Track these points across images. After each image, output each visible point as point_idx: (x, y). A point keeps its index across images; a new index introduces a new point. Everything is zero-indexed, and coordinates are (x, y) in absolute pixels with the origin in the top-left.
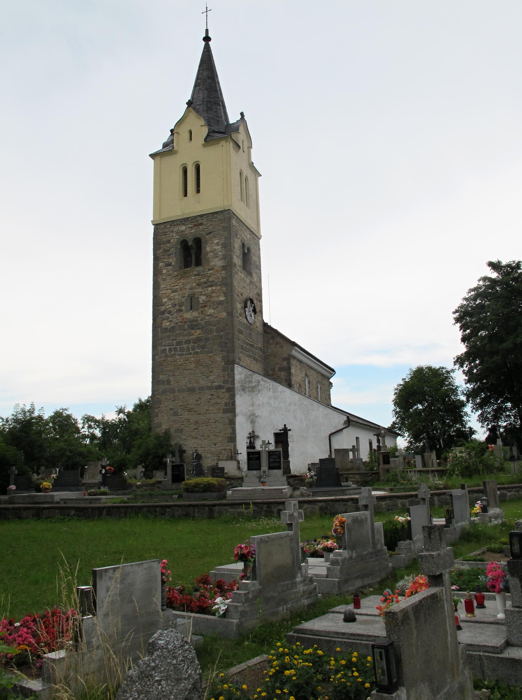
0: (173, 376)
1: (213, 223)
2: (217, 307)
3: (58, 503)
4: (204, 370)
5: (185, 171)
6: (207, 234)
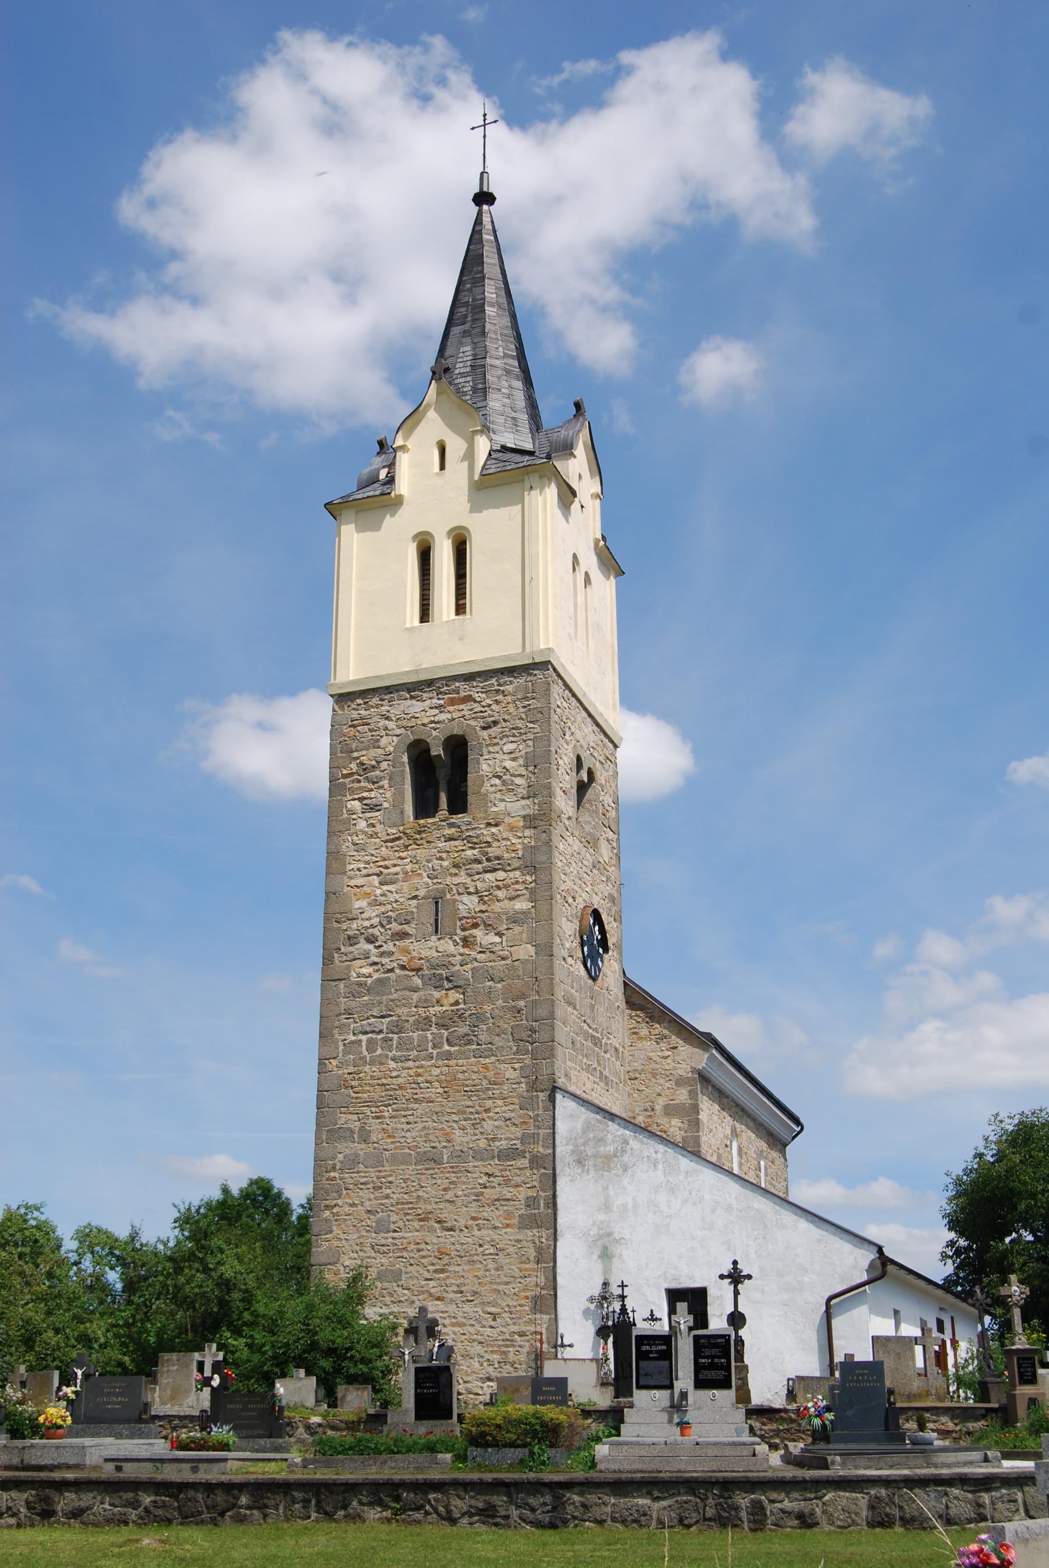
0: (378, 1118)
1: (500, 697)
2: (508, 929)
3: (96, 1468)
4: (469, 1103)
5: (425, 556)
6: (484, 728)
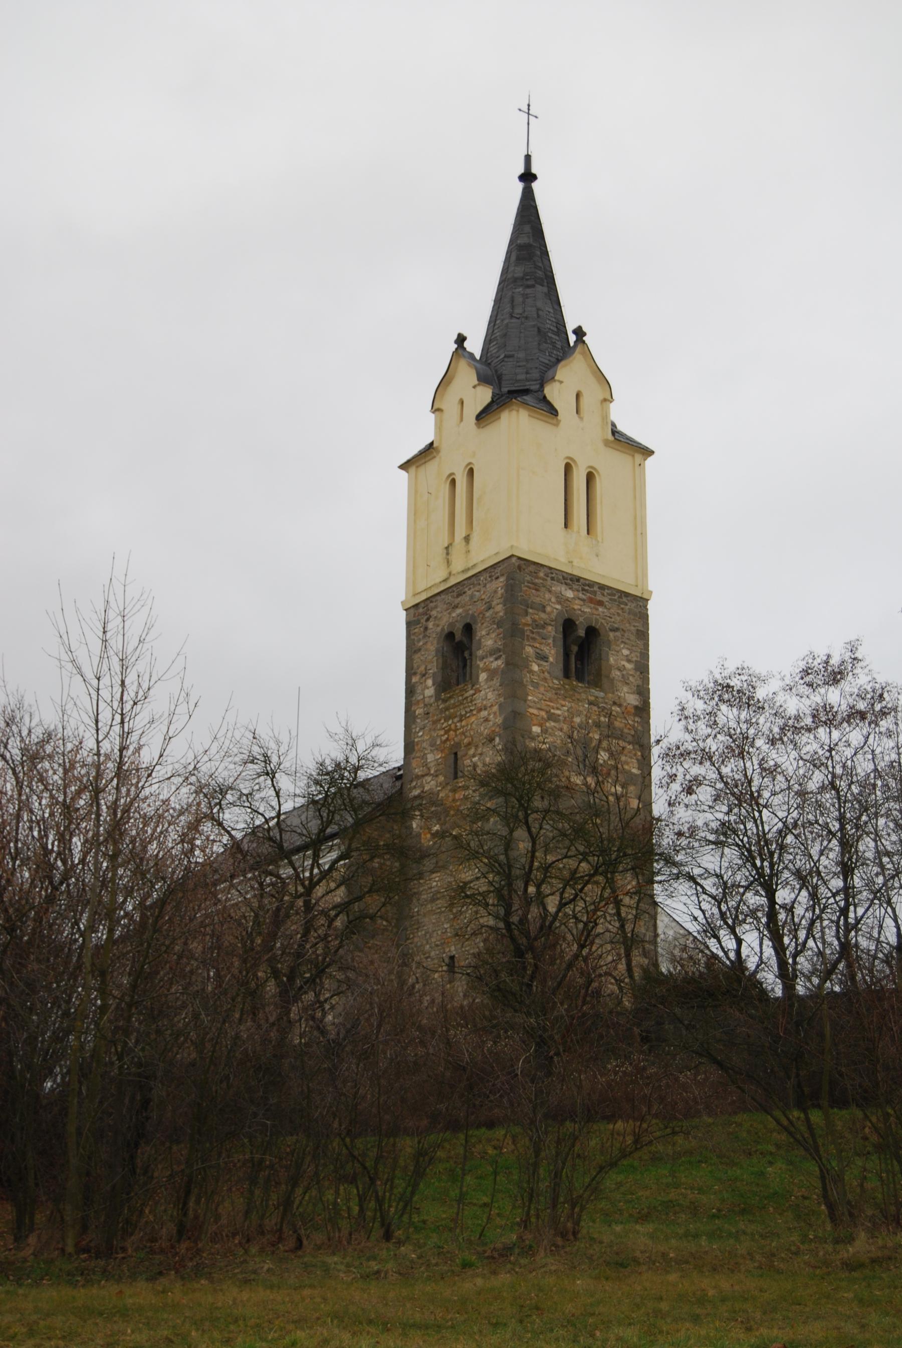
6: (611, 630)
